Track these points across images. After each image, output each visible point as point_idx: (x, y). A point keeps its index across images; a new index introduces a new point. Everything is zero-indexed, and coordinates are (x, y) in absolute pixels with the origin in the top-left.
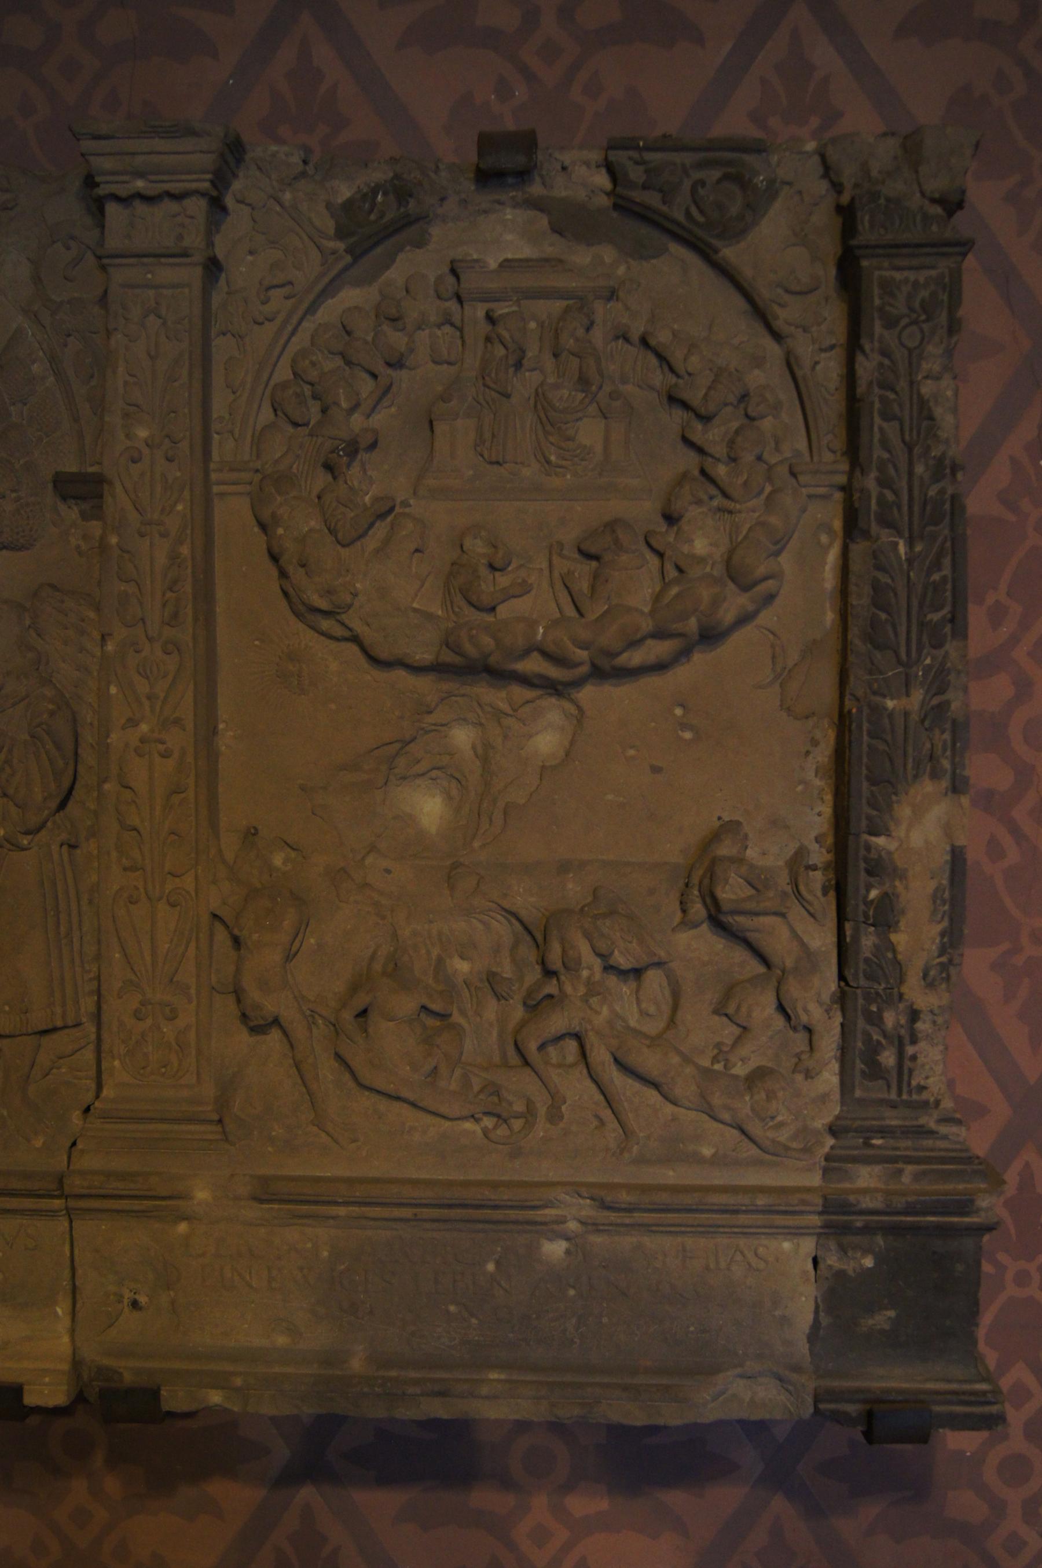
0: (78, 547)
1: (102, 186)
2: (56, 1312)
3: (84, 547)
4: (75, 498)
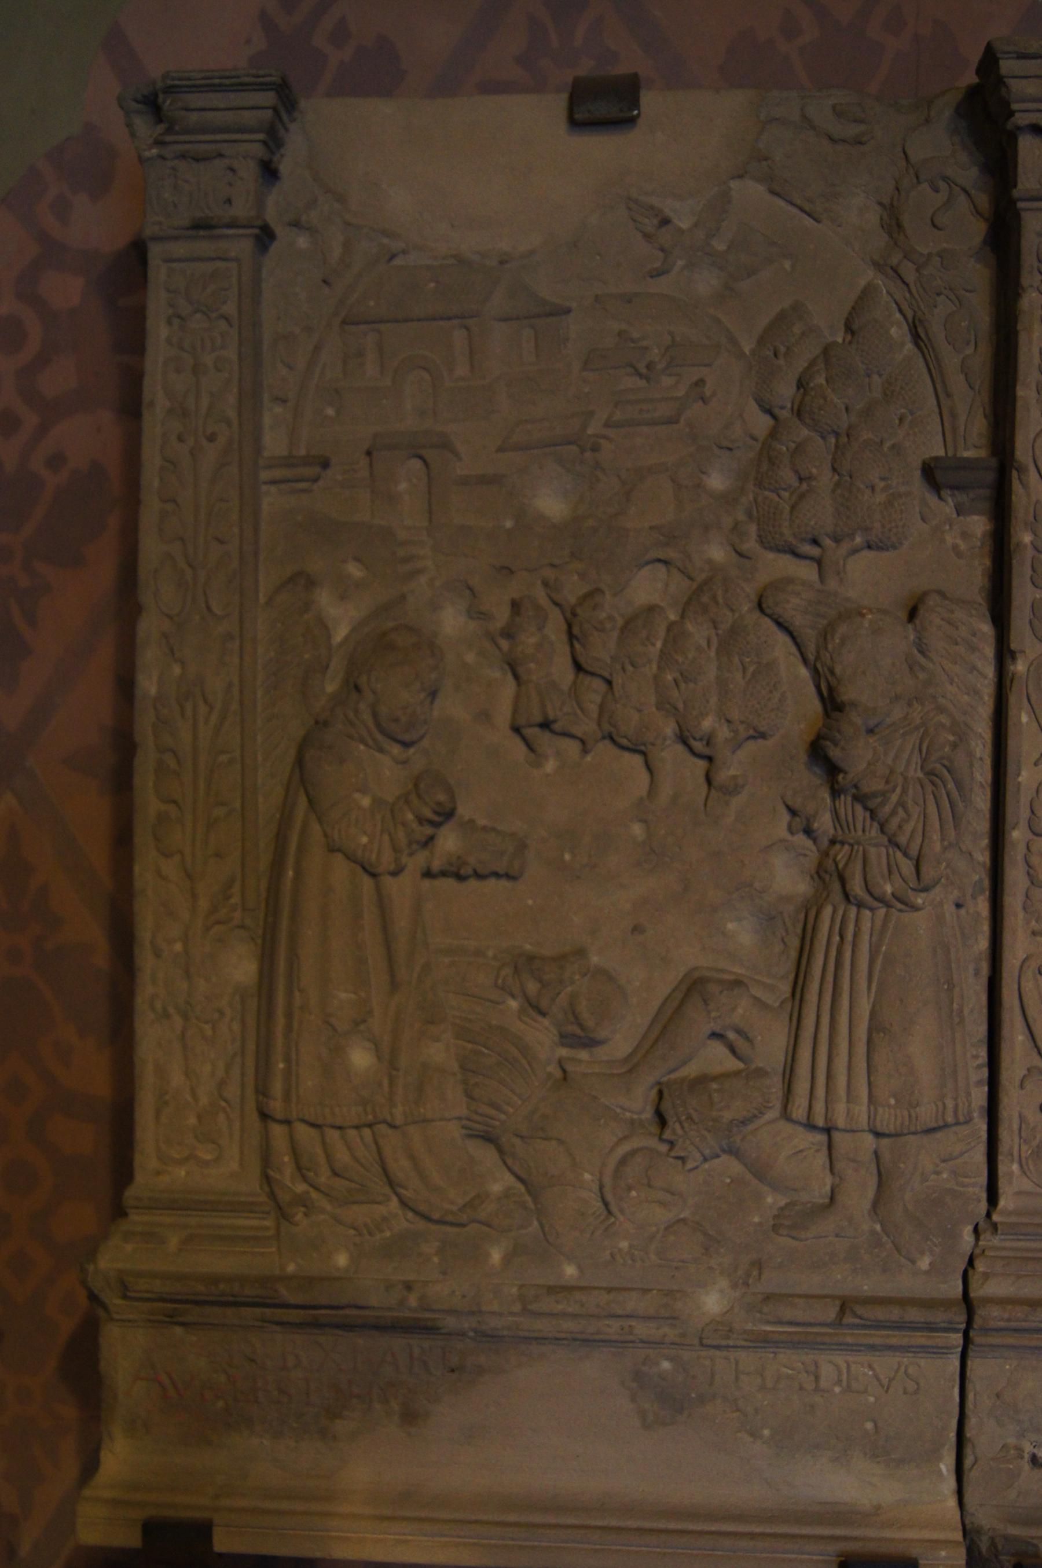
0: (955, 547)
1: (1017, 115)
2: (940, 1471)
3: (963, 546)
4: (952, 488)
